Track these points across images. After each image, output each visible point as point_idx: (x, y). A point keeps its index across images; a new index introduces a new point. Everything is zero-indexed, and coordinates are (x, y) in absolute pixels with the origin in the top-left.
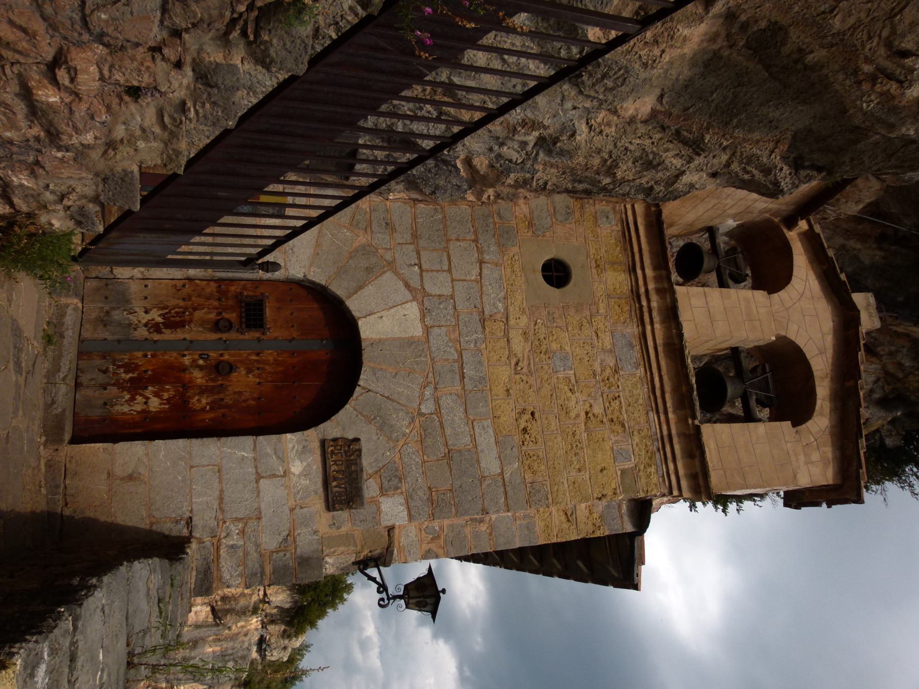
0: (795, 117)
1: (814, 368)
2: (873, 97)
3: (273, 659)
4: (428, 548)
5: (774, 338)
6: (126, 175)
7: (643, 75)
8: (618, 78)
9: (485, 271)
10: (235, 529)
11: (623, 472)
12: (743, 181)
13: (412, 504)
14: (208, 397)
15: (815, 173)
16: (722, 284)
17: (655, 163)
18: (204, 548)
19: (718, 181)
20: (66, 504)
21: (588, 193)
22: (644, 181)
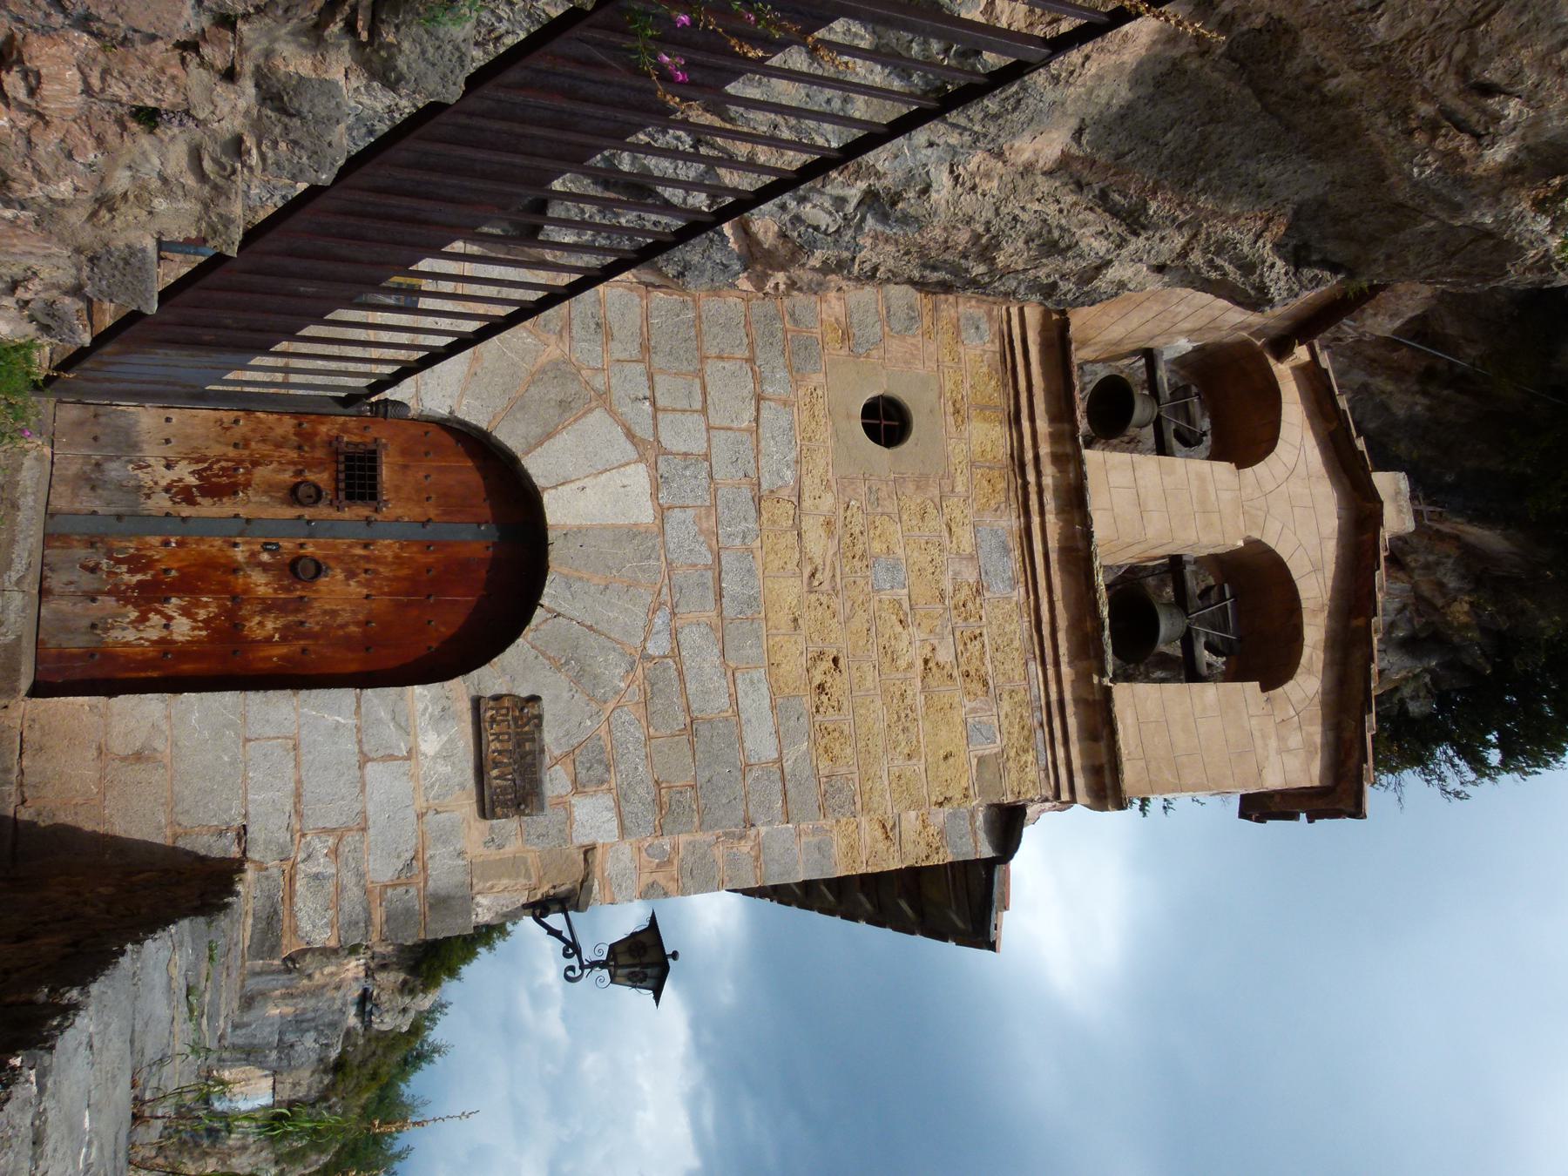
0: (1300, 180)
1: (1303, 595)
2: (1430, 159)
3: (384, 1028)
4: (650, 881)
5: (1241, 543)
6: (133, 254)
7: (1051, 95)
8: (1007, 99)
9: (764, 414)
10: (321, 846)
11: (981, 760)
12: (1208, 280)
13: (626, 808)
14: (276, 618)
15: (1327, 274)
16: (1162, 449)
17: (1062, 245)
18: (267, 878)
19: (1166, 279)
20: (23, 802)
21: (946, 287)
22: (1042, 273)
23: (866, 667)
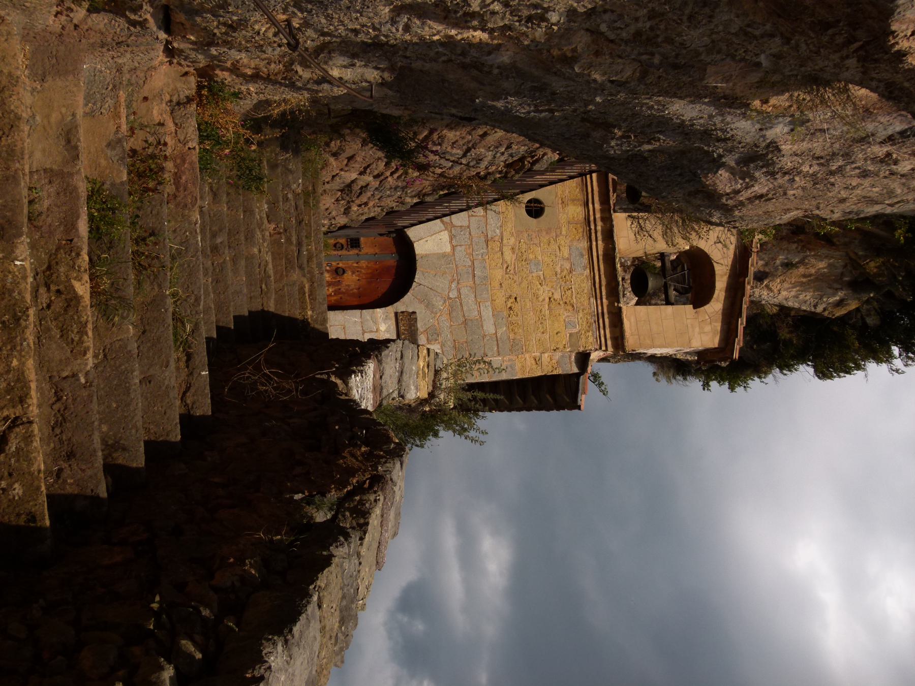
11: (571, 335)
23: (527, 300)
